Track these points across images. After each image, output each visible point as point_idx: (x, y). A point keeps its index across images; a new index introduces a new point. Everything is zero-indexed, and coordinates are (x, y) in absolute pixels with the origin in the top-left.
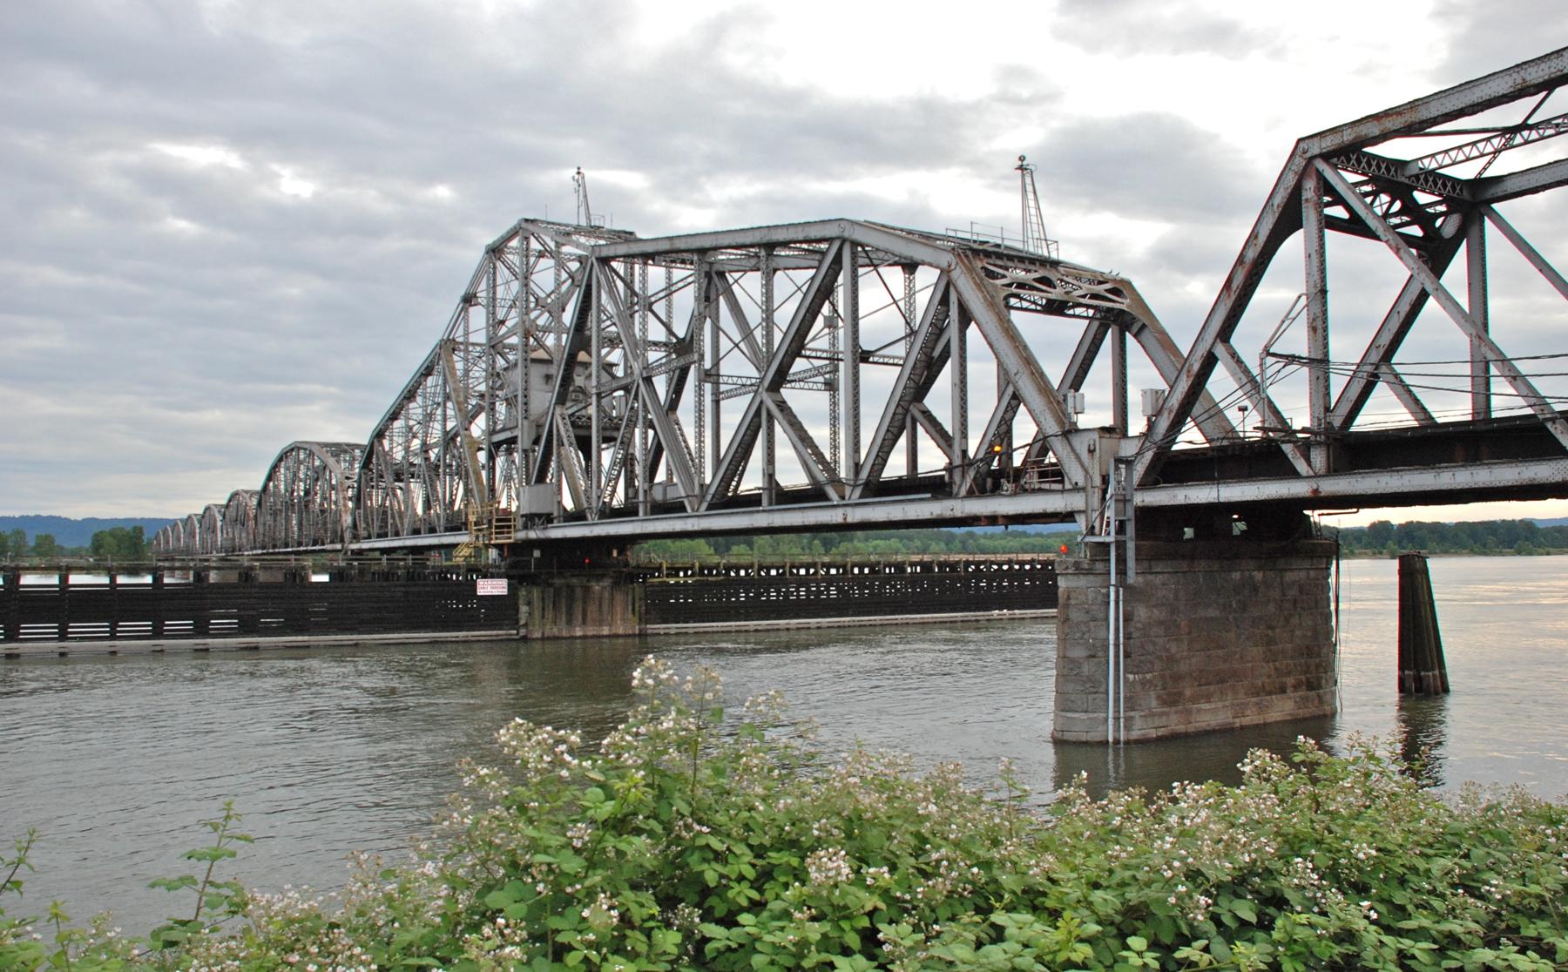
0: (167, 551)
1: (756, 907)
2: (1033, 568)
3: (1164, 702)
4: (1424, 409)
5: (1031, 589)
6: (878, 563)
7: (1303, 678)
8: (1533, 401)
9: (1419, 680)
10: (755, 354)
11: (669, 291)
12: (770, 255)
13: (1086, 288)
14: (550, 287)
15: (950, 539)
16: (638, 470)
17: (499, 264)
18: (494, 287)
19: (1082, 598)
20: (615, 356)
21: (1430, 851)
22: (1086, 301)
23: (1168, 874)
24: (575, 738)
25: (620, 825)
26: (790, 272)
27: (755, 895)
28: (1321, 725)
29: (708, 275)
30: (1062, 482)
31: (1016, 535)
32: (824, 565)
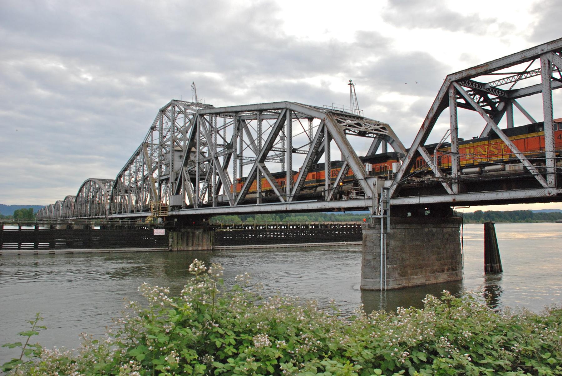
1: (235, 355)
2: (355, 227)
3: (401, 275)
5: (353, 234)
6: (299, 225)
9: (492, 267)
10: (255, 149)
11: (225, 126)
12: (261, 114)
13: (373, 127)
14: (182, 124)
15: (325, 217)
16: (213, 190)
17: (164, 116)
18: (162, 124)
20: (205, 149)
22: (373, 131)
25: (183, 324)
26: (268, 120)
28: (455, 286)
29: (239, 121)
30: (364, 196)
31: (348, 215)
32: (279, 225)
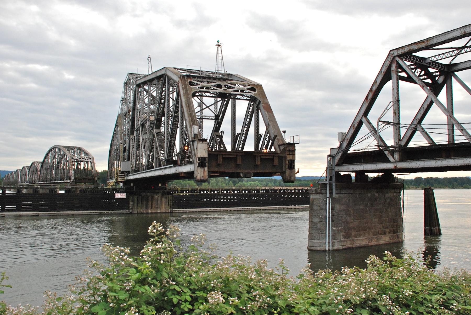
0: (9, 182)
3: (345, 237)
4: (432, 140)
7: (392, 229)
8: (468, 137)
9: (431, 230)
19: (318, 202)
21: (432, 292)
23: (336, 301)
24: (127, 251)
27: (190, 307)
